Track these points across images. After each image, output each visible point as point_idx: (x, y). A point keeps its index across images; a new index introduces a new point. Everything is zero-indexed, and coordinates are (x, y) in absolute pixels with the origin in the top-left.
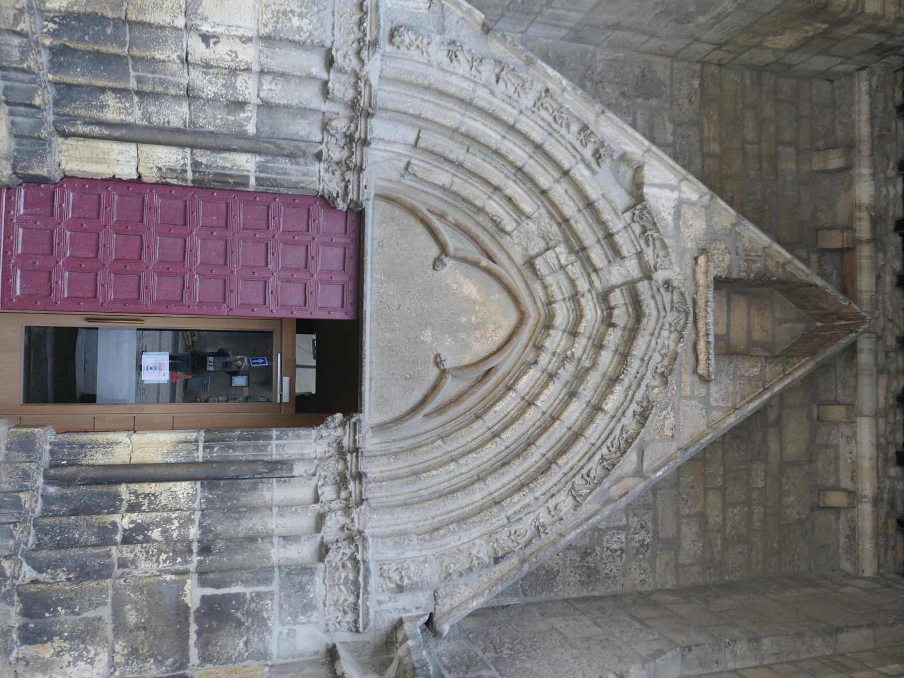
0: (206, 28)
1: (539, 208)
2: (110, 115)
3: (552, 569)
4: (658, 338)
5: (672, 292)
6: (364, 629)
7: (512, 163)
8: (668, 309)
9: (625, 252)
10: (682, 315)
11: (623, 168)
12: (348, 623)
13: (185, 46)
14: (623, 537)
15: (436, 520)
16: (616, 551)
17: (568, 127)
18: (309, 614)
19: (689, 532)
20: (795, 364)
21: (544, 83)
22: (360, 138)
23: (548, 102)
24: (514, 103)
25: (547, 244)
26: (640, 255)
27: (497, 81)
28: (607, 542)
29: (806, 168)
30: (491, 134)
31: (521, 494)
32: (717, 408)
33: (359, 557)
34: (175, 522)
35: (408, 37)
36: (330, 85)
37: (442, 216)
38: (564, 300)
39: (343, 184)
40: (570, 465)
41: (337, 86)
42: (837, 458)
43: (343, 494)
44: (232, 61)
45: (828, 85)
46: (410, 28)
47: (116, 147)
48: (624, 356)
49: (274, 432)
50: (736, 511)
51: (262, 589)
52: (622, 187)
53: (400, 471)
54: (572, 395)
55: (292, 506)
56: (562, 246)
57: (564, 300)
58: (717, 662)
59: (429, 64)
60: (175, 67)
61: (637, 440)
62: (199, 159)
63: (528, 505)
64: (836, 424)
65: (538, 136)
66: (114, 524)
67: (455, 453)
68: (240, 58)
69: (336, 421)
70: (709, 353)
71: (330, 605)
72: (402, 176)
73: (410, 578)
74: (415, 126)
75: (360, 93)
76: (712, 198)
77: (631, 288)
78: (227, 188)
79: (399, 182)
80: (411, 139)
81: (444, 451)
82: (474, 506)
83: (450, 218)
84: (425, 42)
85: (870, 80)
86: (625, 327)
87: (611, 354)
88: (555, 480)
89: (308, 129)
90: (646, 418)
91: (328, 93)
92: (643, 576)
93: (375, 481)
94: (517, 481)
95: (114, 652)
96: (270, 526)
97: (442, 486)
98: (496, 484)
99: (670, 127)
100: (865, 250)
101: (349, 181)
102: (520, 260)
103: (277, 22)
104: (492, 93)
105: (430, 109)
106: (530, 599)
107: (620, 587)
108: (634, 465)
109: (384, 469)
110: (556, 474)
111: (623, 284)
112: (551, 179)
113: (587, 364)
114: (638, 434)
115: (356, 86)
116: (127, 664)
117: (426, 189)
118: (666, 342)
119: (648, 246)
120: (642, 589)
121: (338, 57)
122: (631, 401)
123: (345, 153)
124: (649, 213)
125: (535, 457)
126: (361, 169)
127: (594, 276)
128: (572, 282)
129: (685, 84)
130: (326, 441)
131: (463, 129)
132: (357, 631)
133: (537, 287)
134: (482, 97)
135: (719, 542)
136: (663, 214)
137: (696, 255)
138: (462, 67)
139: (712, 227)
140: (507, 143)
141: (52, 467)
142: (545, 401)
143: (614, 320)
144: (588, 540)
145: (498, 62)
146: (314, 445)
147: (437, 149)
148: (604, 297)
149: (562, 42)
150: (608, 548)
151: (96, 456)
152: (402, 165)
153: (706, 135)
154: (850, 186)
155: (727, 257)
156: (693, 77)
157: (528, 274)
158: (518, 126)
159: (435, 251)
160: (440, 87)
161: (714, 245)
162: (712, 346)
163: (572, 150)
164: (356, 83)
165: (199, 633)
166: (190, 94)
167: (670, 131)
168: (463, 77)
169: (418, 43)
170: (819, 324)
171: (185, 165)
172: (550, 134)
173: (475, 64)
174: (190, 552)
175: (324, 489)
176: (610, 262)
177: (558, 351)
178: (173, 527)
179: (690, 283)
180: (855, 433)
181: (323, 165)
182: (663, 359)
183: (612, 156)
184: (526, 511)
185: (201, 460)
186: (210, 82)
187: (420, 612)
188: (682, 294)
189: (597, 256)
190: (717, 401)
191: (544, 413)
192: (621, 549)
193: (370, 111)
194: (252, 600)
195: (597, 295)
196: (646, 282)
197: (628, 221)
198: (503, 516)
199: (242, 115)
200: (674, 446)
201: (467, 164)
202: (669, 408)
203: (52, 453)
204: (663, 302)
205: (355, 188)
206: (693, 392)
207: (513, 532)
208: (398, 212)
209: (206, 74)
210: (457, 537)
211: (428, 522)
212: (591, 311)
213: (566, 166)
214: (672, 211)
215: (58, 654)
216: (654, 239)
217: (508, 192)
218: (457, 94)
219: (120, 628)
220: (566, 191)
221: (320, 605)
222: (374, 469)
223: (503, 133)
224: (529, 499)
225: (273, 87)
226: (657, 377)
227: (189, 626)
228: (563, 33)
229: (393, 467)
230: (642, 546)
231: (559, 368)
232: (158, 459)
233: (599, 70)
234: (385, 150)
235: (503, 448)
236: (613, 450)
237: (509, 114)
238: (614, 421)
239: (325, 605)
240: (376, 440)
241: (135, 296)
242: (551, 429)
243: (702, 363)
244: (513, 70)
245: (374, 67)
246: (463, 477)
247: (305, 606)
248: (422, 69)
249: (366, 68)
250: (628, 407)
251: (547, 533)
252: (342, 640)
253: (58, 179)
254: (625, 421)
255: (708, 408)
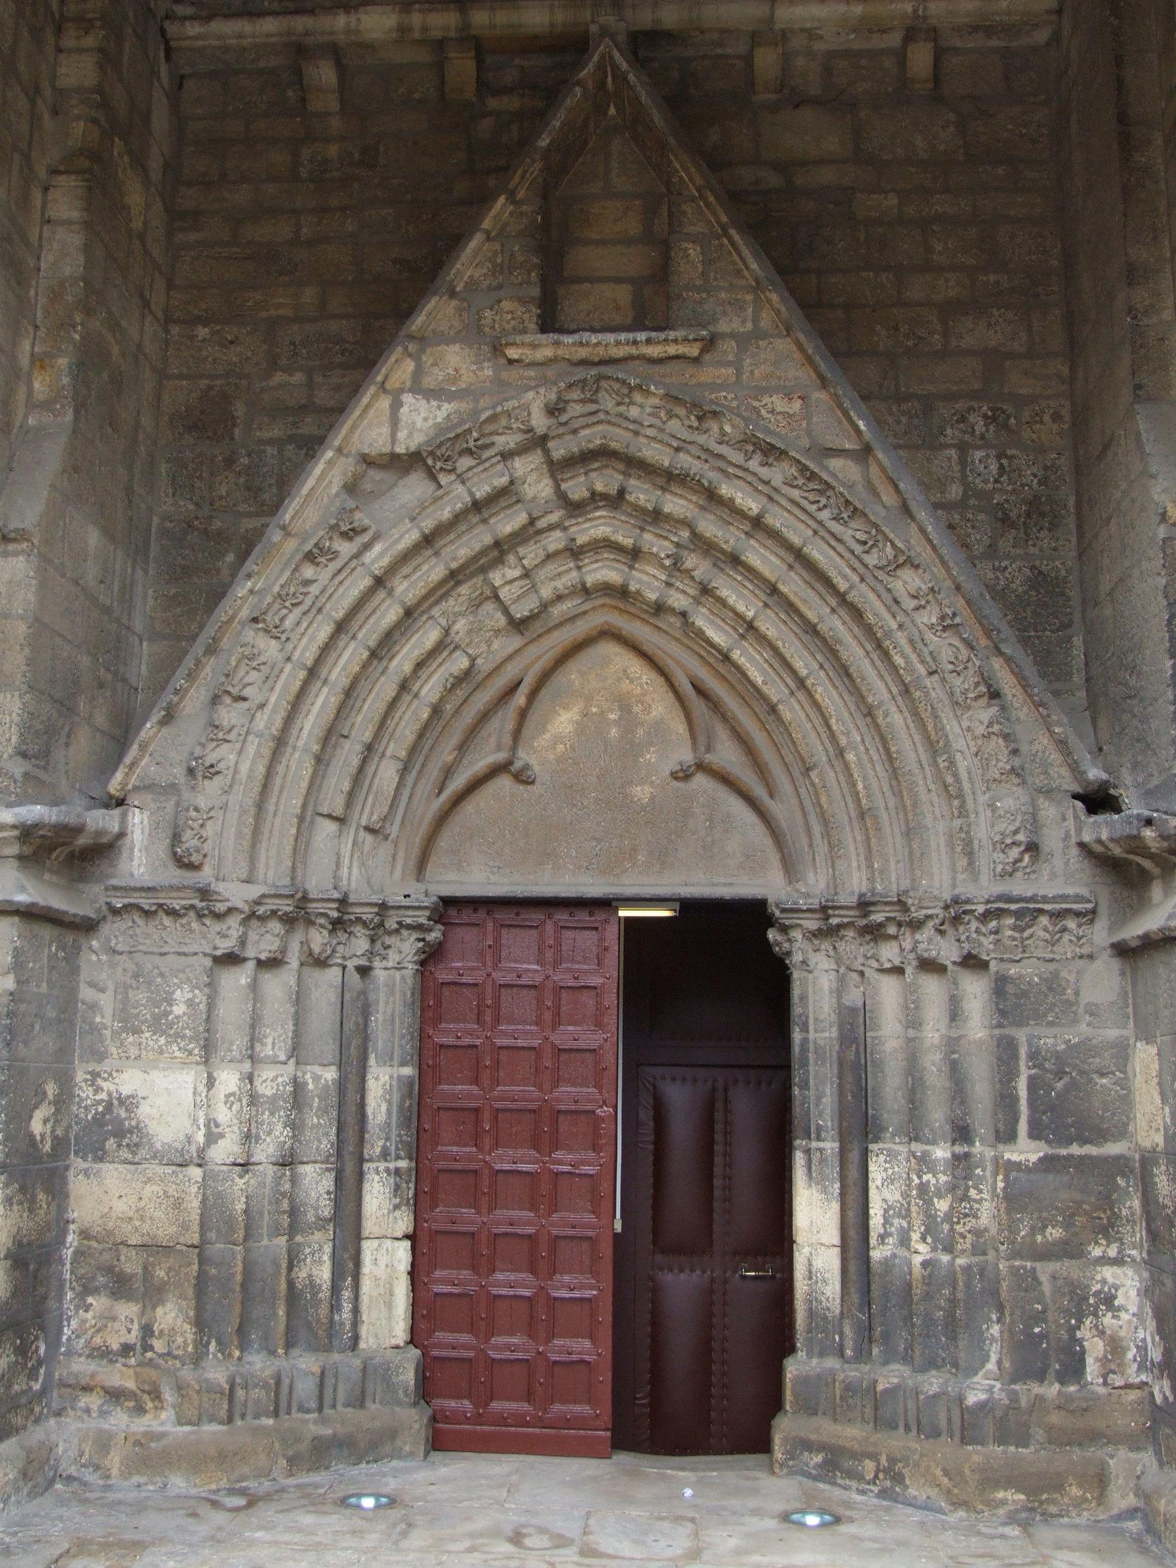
0: (200, 1138)
1: (431, 618)
2: (324, 1274)
3: (1029, 579)
4: (641, 424)
5: (567, 402)
6: (1089, 901)
7: (365, 666)
8: (594, 407)
9: (504, 480)
10: (604, 384)
11: (367, 486)
12: (1080, 926)
13: (225, 1168)
14: (979, 454)
15: (932, 787)
16: (1001, 467)
17: (307, 583)
18: (1063, 983)
19: (974, 334)
20: (681, 178)
21: (242, 624)
22: (338, 910)
23: (271, 619)
24: (276, 671)
25: (487, 598)
26: (506, 456)
27: (245, 699)
28: (986, 482)
29: (336, 123)
30: (322, 702)
31: (892, 652)
32: (756, 320)
33: (981, 909)
34: (925, 1178)
35: (189, 840)
36: (263, 957)
37: (448, 772)
38: (579, 568)
39: (405, 933)
40: (848, 571)
41: (263, 946)
42: (846, 54)
43: (892, 930)
44: (240, 1100)
45: (190, 84)
46: (176, 838)
47: (367, 1268)
48: (670, 478)
49: (797, 1036)
50: (939, 248)
51: (1023, 1052)
52: (395, 485)
53: (859, 838)
54: (735, 560)
55: (907, 1008)
56: (491, 575)
57: (579, 568)
58: (1162, 339)
59: (224, 807)
60: (252, 1182)
61: (808, 463)
62: (378, 1150)
63: (911, 642)
64: (786, 58)
65: (324, 632)
66: (925, 1264)
67: (831, 749)
68: (234, 1089)
69: (779, 938)
70: (666, 340)
71: (1052, 952)
72: (386, 838)
73: (1016, 832)
74: (312, 822)
75: (274, 912)
76: (412, 337)
77: (557, 468)
78: (423, 1112)
79: (396, 843)
80: (331, 827)
81: (828, 768)
82: (912, 725)
83: (450, 758)
84: (193, 814)
85: (184, 19)
86: (623, 473)
87: (668, 497)
88: (872, 596)
89: (325, 986)
90: (773, 447)
91: (275, 959)
92: (1047, 418)
93: (871, 880)
94: (874, 656)
95: (1103, 1257)
96: (936, 1041)
97: (882, 774)
98: (879, 689)
99: (278, 378)
100: (480, 18)
101: (399, 923)
102: (516, 642)
103: (183, 1037)
104: (262, 706)
105: (288, 801)
106: (1077, 617)
107: (1063, 458)
108: (850, 463)
109: (854, 864)
110: (862, 595)
111: (553, 476)
112: (388, 602)
113: (685, 534)
114: (798, 462)
115: (262, 919)
116: (1121, 1239)
117: (404, 798)
118: (648, 410)
119: (493, 444)
120: (1067, 418)
121: (225, 946)
122: (747, 470)
123: (358, 930)
124: (439, 446)
125: (837, 626)
126: (383, 907)
127: (541, 524)
128: (549, 557)
129: (204, 353)
130: (811, 954)
131: (316, 748)
132: (1094, 912)
133: (558, 611)
134: (268, 721)
135: (992, 278)
136: (439, 420)
137: (503, 361)
138: (224, 755)
139: (458, 333)
140: (333, 676)
141: (842, 1354)
142: (746, 603)
143: (613, 491)
144: (982, 517)
145: (215, 700)
146: (816, 973)
147: (346, 786)
148: (575, 508)
149: (151, 572)
150: (996, 481)
151: (829, 1294)
152: (369, 839)
153: (288, 312)
154: (368, 47)
155: (506, 305)
156: (192, 338)
157: (537, 627)
158: (309, 663)
159: (504, 782)
160: (257, 789)
161: (487, 330)
162: (654, 334)
163: (344, 574)
164: (259, 918)
165: (1084, 1141)
166: (288, 1161)
167: (286, 377)
168: (240, 753)
169: (196, 825)
170: (612, 111)
171: (387, 1170)
172: (320, 610)
173: (221, 736)
174: (967, 1155)
175: (883, 959)
176: (518, 501)
177: (664, 578)
178: (933, 1181)
179: (550, 373)
180: (802, 30)
181: (377, 963)
182: (677, 416)
183: (351, 511)
184: (919, 645)
185: (836, 1145)
186: (269, 1133)
187: (1070, 814)
188: (570, 386)
189: (508, 523)
190: (744, 322)
191: (766, 605)
192: (998, 457)
193: (299, 895)
194: (1039, 1066)
195: (572, 517)
196: (550, 445)
197: (453, 477)
198: (928, 682)
199: (311, 1087)
200: (820, 395)
201: (367, 736)
202: (756, 404)
203: (822, 1354)
204: (582, 416)
205: (410, 913)
206: (728, 364)
207: (951, 667)
208: (444, 842)
209: (258, 1138)
210: (958, 756)
211: (935, 799)
212: (598, 526)
213: (367, 582)
214: (434, 403)
215: (1101, 1333)
216: (483, 435)
217: (408, 668)
218: (266, 761)
219: (1070, 1250)
220: (405, 577)
221: (1052, 966)
222: (855, 881)
223: (319, 684)
224: (901, 638)
225: (269, 1041)
226: (706, 425)
227: (1072, 1156)
228: (139, 573)
229: (852, 848)
230: (994, 419)
231: (692, 578)
232: (835, 1206)
233: (192, 507)
234: (350, 867)
235: (822, 673)
236: (823, 501)
237: (291, 678)
238: (776, 497)
239: (1052, 960)
240: (811, 877)
241: (585, 1245)
242: (792, 597)
243: (681, 349)
244: (227, 676)
245: (236, 894)
246: (868, 740)
247: (1050, 989)
248: (233, 817)
249: (240, 904)
250: (755, 474)
251: (954, 615)
252: (1105, 934)
253: (418, 1352)
254: (777, 479)
255: (757, 335)
